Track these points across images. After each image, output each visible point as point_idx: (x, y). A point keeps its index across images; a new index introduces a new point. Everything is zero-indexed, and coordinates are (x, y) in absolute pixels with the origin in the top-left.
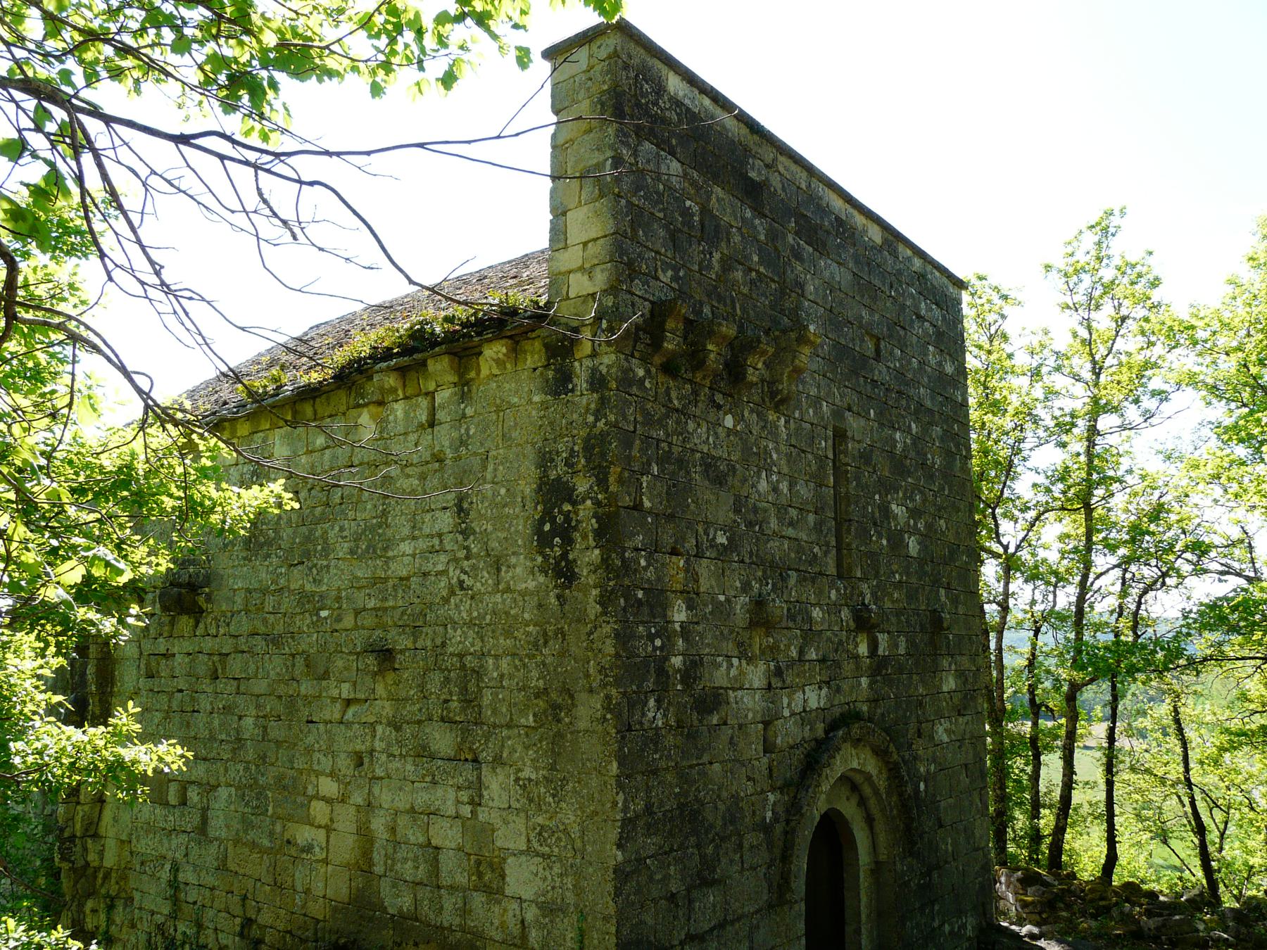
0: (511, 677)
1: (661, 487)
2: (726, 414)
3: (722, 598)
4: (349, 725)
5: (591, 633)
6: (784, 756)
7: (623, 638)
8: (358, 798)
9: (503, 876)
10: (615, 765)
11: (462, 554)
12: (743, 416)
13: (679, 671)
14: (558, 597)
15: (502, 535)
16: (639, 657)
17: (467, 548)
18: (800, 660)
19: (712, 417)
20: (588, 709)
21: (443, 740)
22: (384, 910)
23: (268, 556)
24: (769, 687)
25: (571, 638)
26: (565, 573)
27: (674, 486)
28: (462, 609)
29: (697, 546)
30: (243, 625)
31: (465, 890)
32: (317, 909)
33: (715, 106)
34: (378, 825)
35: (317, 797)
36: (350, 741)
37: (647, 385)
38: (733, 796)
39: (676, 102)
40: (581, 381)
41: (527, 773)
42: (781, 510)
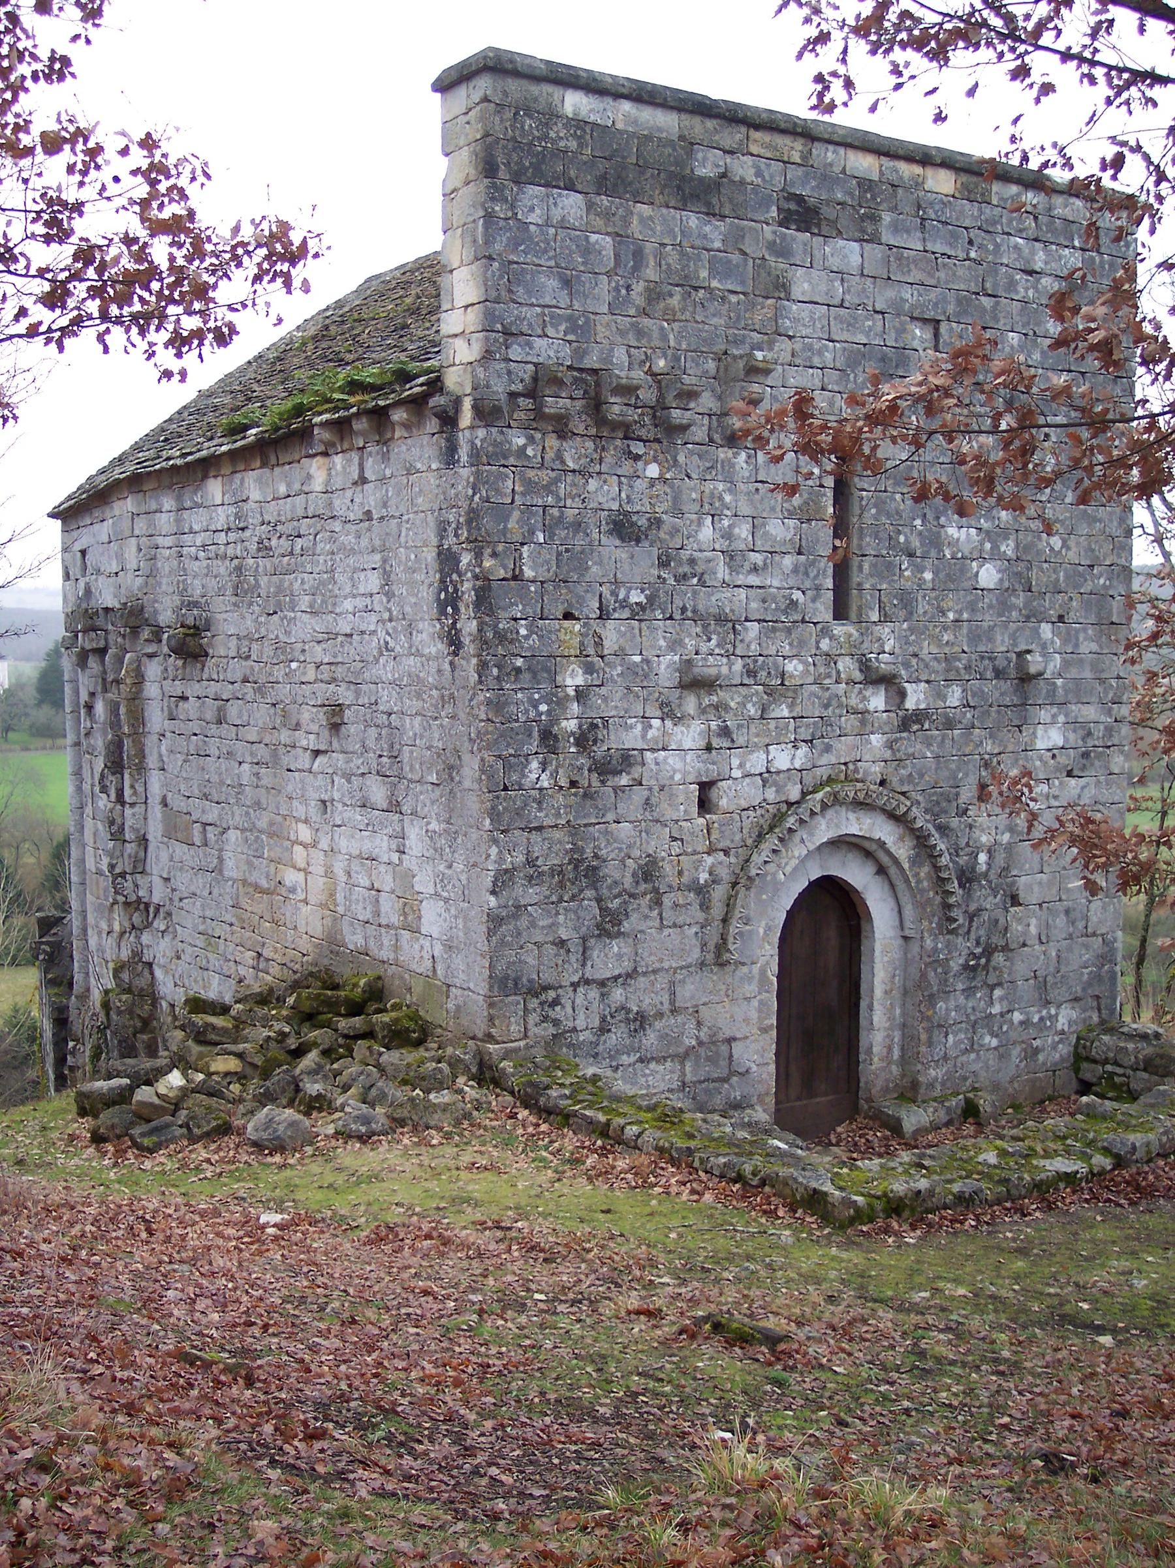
0: (421, 737)
1: (548, 555)
2: (647, 463)
3: (637, 659)
4: (315, 774)
5: (471, 700)
6: (732, 819)
7: (497, 706)
8: (324, 844)
9: (420, 918)
10: (488, 821)
11: (386, 616)
12: (676, 461)
13: (573, 734)
14: (451, 663)
15: (413, 600)
16: (517, 721)
17: (389, 610)
18: (762, 718)
19: (627, 467)
20: (470, 768)
21: (378, 793)
22: (345, 945)
23: (251, 604)
24: (709, 748)
25: (459, 704)
26: (454, 641)
27: (567, 550)
28: (385, 670)
29: (600, 609)
30: (237, 669)
31: (397, 929)
32: (304, 944)
33: (640, 106)
34: (339, 869)
35: (297, 842)
36: (316, 788)
37: (530, 452)
38: (649, 856)
39: (579, 124)
40: (463, 454)
41: (434, 826)
42: (730, 556)
